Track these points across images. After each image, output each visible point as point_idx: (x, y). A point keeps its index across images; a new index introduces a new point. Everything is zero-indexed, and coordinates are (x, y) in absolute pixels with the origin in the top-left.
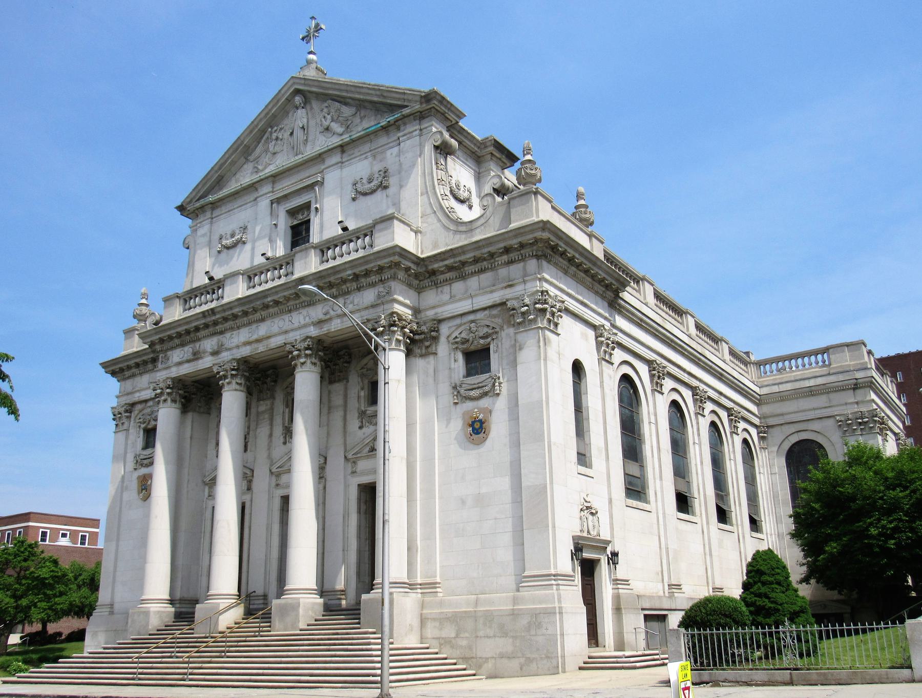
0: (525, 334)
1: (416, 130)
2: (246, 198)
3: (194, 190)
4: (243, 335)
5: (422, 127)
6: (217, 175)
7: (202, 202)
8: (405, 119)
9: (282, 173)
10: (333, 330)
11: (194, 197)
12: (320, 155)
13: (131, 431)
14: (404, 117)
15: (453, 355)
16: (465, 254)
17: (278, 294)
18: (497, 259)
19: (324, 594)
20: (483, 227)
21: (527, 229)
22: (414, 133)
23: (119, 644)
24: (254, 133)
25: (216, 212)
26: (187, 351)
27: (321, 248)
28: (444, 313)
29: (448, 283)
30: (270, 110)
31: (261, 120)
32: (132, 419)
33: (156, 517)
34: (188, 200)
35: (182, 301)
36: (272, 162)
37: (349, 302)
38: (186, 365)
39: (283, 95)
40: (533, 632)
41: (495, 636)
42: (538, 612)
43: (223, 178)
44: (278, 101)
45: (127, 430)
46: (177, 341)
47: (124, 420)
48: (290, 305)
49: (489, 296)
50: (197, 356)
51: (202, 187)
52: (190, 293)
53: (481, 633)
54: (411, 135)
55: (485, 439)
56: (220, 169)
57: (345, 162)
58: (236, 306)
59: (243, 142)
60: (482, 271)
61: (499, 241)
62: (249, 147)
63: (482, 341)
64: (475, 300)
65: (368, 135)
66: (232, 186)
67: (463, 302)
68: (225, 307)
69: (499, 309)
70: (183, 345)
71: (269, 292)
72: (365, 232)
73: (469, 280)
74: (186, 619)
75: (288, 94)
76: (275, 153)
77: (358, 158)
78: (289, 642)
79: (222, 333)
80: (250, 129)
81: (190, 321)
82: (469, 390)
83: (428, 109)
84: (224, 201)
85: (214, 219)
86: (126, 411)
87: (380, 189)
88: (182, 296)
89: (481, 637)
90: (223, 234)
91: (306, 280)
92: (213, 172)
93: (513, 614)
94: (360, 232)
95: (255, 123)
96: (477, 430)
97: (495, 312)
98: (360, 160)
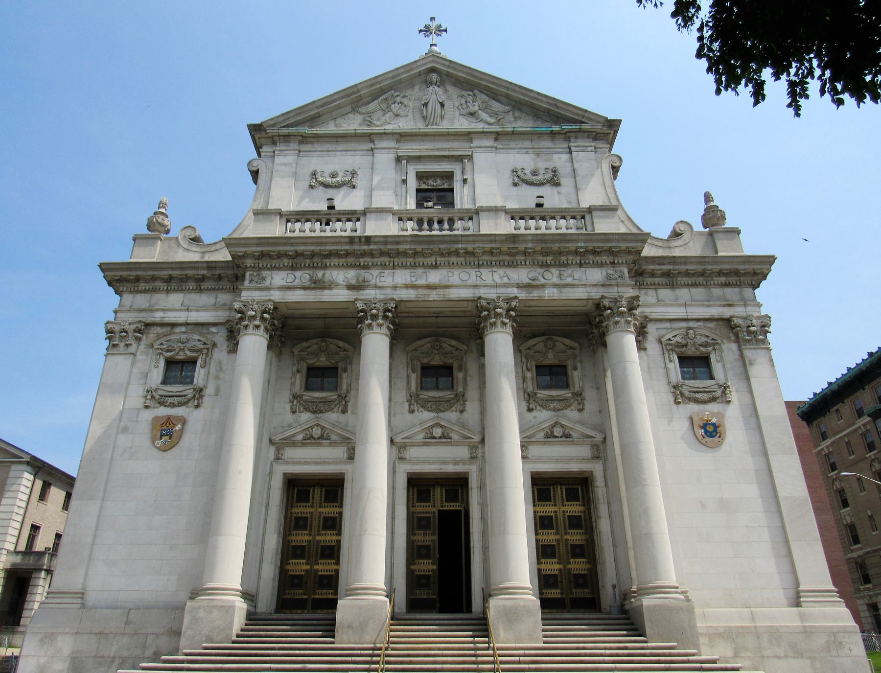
0: (753, 351)
1: (591, 146)
2: (353, 145)
3: (283, 115)
4: (402, 276)
5: (597, 146)
6: (317, 111)
7: (292, 130)
9: (416, 135)
10: (547, 298)
11: (281, 122)
12: (469, 133)
13: (139, 357)
15: (667, 355)
16: (686, 265)
17: (475, 244)
18: (714, 278)
19: (80, 595)
20: (682, 248)
21: (758, 260)
22: (589, 149)
23: (186, 655)
26: (302, 276)
28: (653, 314)
29: (654, 287)
32: (143, 343)
33: (240, 472)
34: (272, 122)
35: (284, 220)
37: (565, 275)
38: (301, 292)
39: (418, 67)
40: (834, 653)
41: (786, 656)
42: (836, 630)
43: (320, 116)
45: (134, 355)
46: (286, 261)
47: (131, 341)
48: (482, 260)
49: (706, 309)
50: (318, 285)
51: (294, 116)
52: (301, 215)
53: (768, 653)
54: (585, 148)
55: (719, 445)
56: (323, 106)
59: (359, 91)
60: (695, 285)
61: (724, 263)
63: (703, 349)
64: (689, 309)
65: (532, 134)
66: (330, 128)
67: (675, 308)
68: (390, 240)
69: (715, 323)
70: (293, 268)
71: (464, 239)
72: (575, 214)
73: (677, 290)
74: (437, 622)
75: (424, 68)
76: (397, 115)
77: (517, 150)
78: (347, 655)
79: (366, 267)
80: (372, 82)
82: (693, 392)
83: (604, 133)
85: (301, 153)
86: (139, 331)
87: (549, 184)
88: (286, 215)
89: (768, 657)
90: (318, 171)
92: (313, 106)
93: (805, 632)
94: (569, 212)
95: (380, 79)
96: (711, 433)
97: (710, 325)
98: (518, 153)
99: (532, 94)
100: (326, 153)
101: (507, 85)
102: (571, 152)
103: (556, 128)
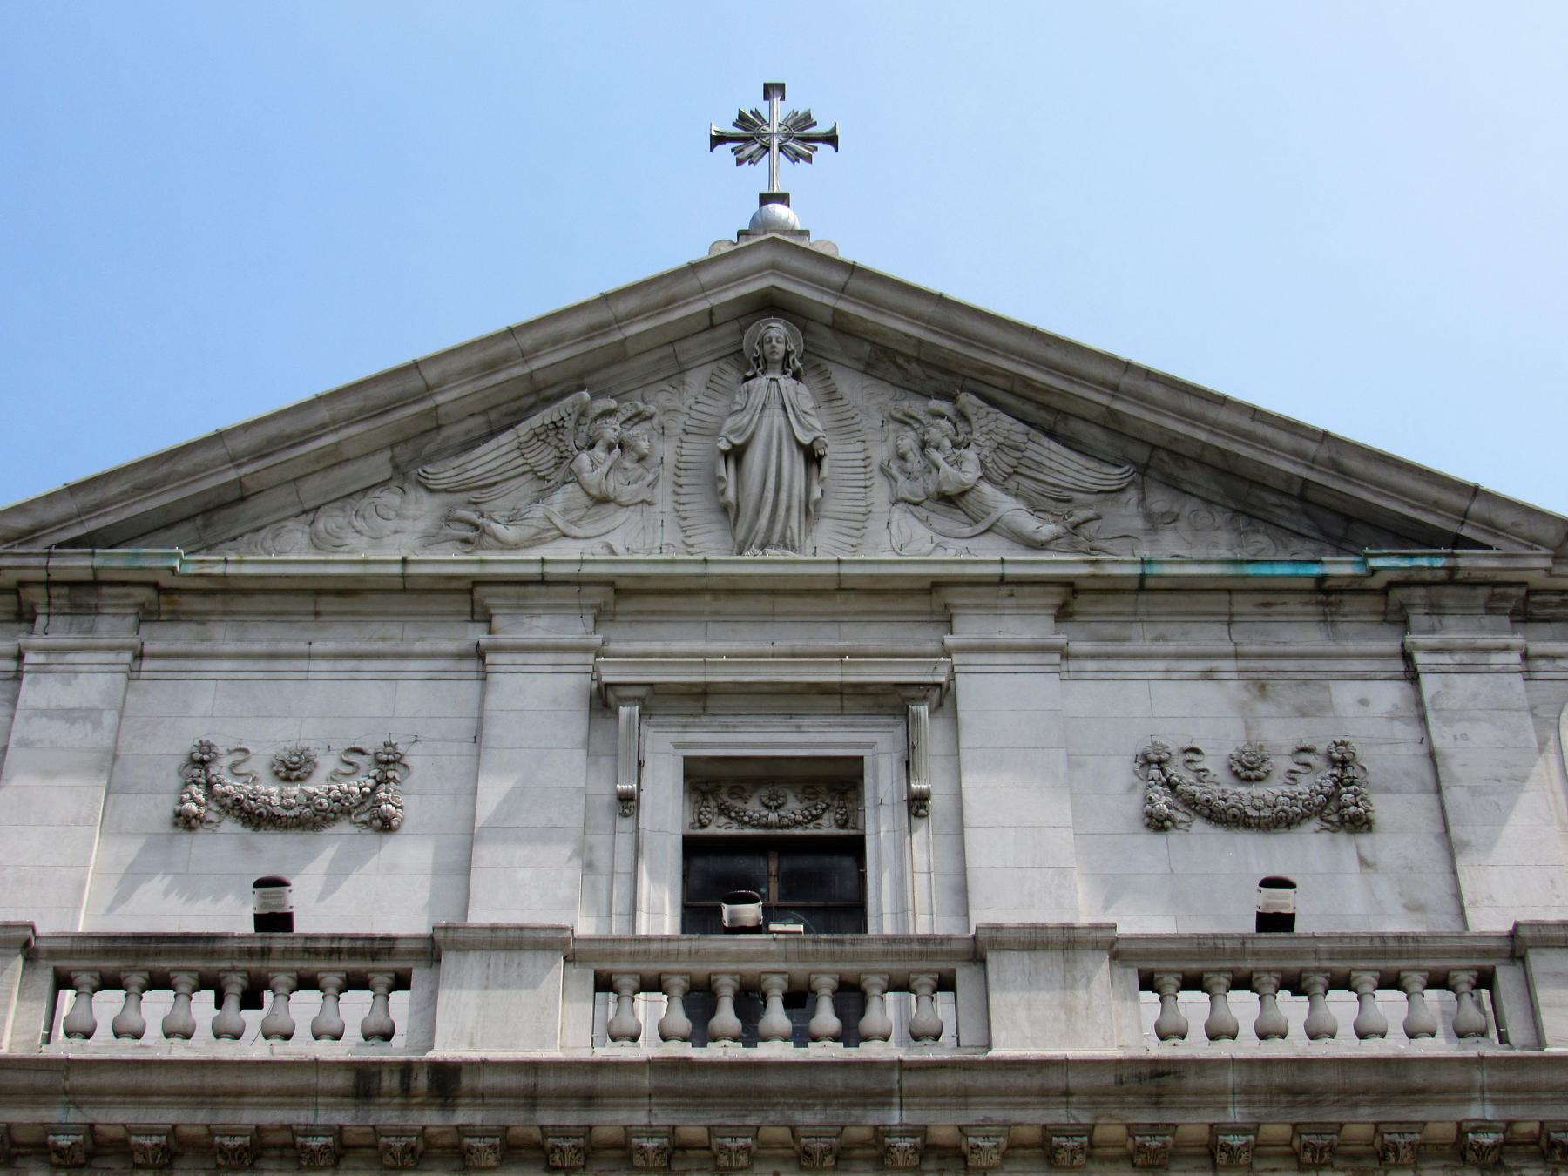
1: (1507, 649)
3: (72, 490)
6: (232, 475)
7: (113, 560)
8: (1450, 590)
11: (62, 523)
12: (936, 585)
14: (1451, 578)
22: (1498, 659)
24: (501, 376)
25: (160, 638)
27: (606, 966)
30: (619, 322)
31: (557, 341)
36: (575, 531)
39: (704, 289)
43: (243, 499)
44: (670, 303)
52: (123, 953)
54: (1482, 658)
56: (259, 454)
57: (1077, 657)
58: (630, 1096)
59: (429, 390)
62: (439, 427)
65: (1230, 591)
68: (550, 1082)
71: (911, 1081)
75: (732, 295)
76: (602, 500)
81: (240, 1093)
84: (241, 604)
85: (147, 665)
88: (53, 954)
91: (1192, 1082)
92: (218, 452)
94: (1416, 954)
95: (527, 341)
99: (1223, 415)
100: (263, 665)
101: (1111, 375)
102: (1412, 676)
103: (1341, 567)
